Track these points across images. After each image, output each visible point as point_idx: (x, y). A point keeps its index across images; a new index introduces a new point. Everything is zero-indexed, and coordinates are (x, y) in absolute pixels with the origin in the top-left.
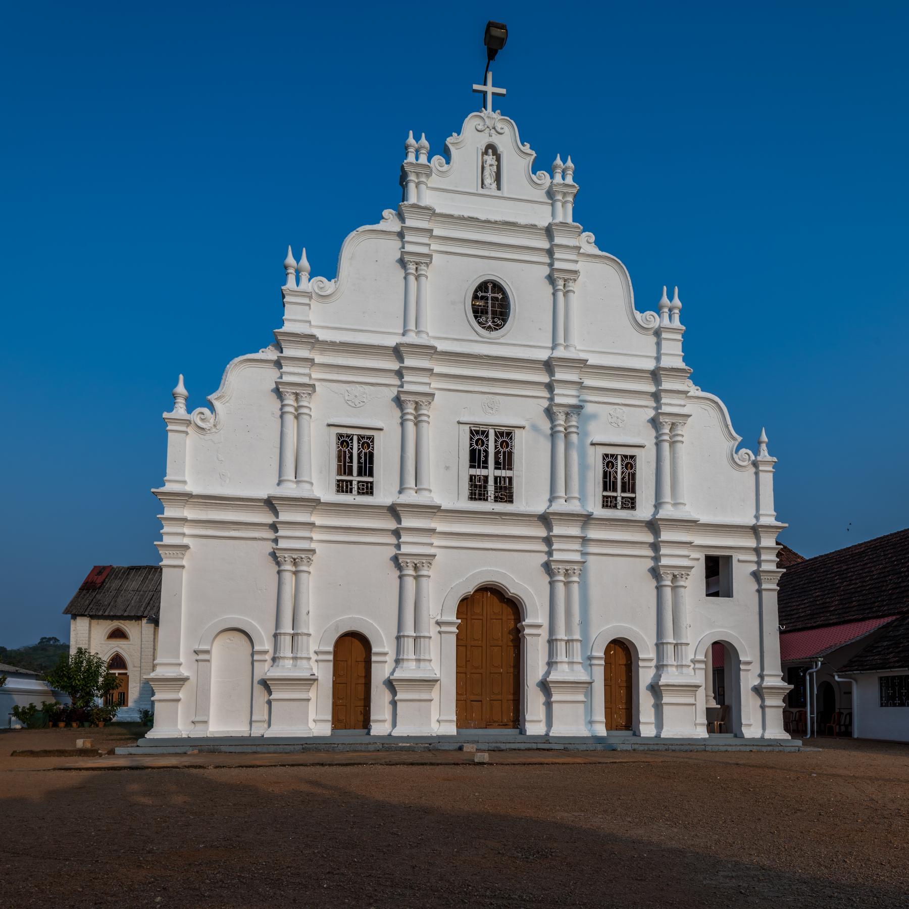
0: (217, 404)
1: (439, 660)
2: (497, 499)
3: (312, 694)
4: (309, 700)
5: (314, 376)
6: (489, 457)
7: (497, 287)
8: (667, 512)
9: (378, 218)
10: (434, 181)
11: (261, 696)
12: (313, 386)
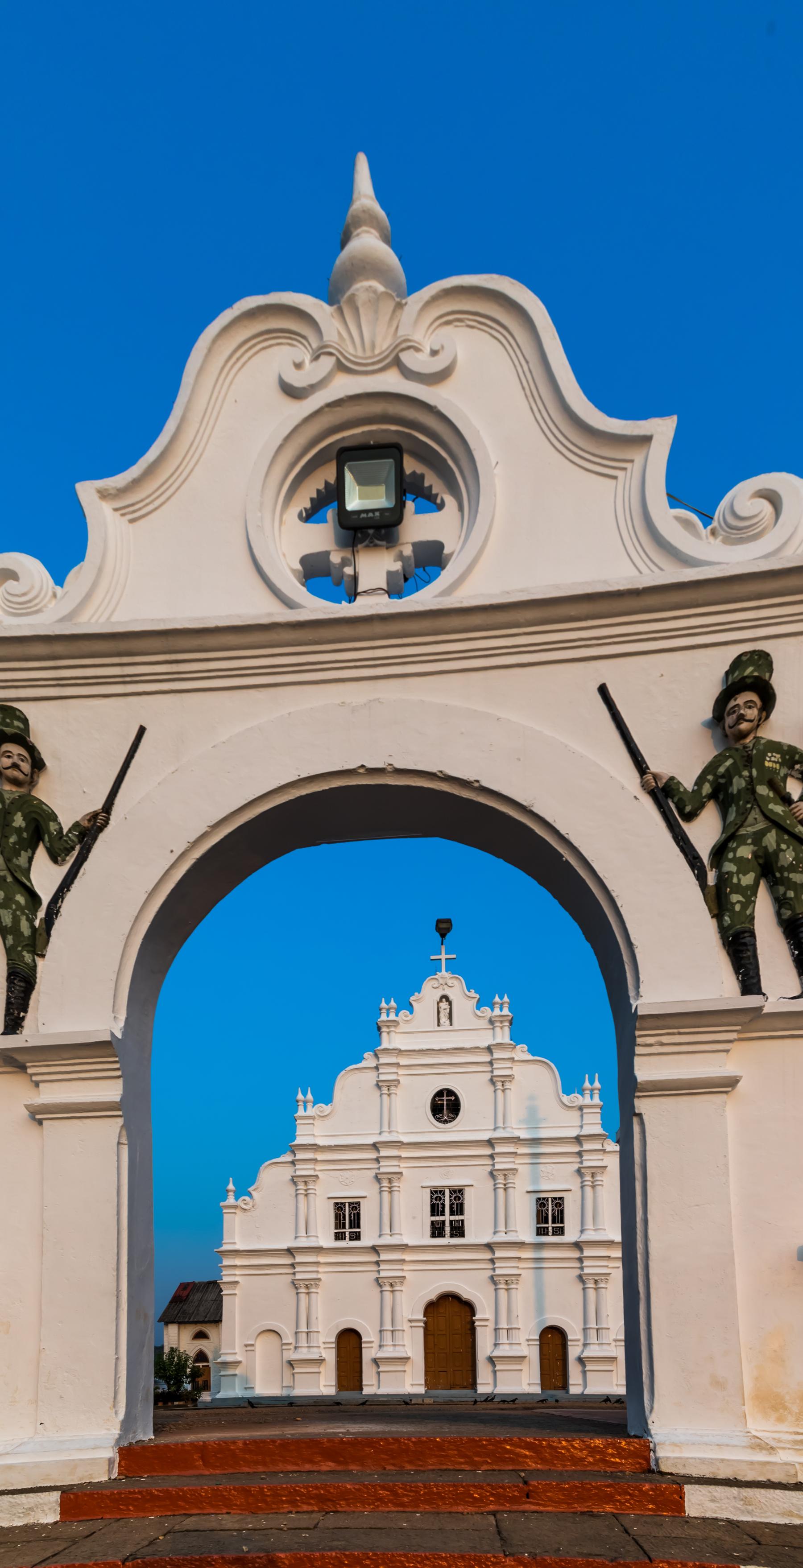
0: (254, 1193)
1: (412, 1345)
2: (452, 1236)
3: (322, 1369)
4: (319, 1373)
5: (400, 1073)
6: (447, 1212)
7: (450, 1092)
8: (590, 1235)
9: (361, 1059)
10: (402, 1027)
11: (287, 1371)
12: (398, 1081)
